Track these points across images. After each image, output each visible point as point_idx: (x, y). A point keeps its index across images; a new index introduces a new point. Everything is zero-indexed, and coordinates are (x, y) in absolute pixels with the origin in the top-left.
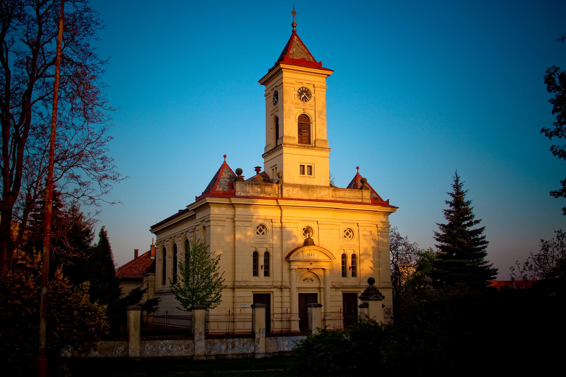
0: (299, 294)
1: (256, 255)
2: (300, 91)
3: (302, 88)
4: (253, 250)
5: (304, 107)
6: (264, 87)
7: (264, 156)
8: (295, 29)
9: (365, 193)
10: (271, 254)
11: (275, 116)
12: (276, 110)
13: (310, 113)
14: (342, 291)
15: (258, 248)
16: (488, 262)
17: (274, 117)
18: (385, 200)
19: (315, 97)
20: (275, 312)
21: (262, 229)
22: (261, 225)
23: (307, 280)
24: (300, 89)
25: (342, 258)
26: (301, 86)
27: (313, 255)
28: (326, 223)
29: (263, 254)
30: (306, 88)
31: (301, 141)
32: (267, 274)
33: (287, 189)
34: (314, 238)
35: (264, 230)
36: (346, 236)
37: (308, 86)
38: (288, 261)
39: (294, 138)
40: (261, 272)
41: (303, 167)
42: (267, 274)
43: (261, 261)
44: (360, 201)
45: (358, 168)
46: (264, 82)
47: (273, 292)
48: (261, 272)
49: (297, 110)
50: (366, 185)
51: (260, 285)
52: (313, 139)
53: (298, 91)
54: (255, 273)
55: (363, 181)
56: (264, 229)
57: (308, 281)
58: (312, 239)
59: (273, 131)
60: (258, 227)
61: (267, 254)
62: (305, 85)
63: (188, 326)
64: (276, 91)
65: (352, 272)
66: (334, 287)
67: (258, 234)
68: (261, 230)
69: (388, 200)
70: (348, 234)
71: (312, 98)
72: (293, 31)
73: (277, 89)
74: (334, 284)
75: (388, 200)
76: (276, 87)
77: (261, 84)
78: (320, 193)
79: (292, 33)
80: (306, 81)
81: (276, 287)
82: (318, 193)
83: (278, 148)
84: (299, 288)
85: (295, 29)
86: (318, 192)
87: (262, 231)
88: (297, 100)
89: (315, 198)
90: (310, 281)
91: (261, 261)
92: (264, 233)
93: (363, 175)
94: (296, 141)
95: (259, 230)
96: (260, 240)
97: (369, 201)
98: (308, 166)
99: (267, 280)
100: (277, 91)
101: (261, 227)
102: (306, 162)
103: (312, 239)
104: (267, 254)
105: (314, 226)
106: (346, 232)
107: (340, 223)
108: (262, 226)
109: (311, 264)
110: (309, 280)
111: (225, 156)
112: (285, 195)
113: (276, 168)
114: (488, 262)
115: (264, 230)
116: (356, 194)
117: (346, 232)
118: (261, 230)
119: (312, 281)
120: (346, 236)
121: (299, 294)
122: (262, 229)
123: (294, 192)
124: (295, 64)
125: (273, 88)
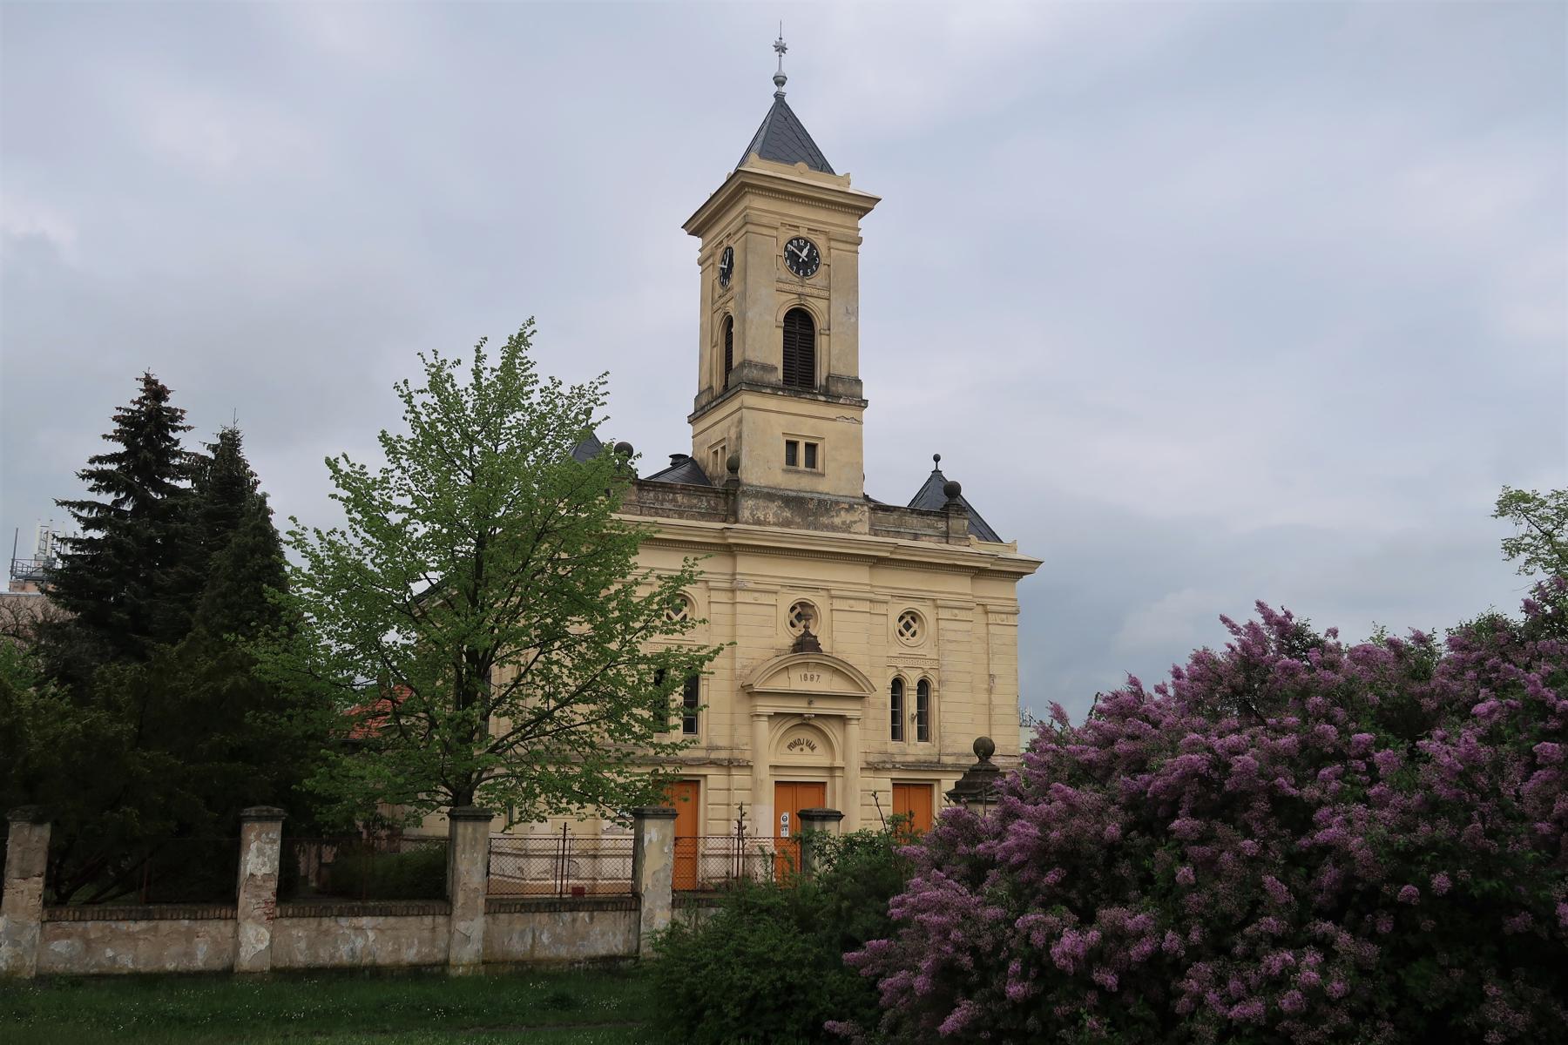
0: (776, 782)
1: (897, 684)
4: (892, 674)
5: (800, 290)
6: (697, 242)
7: (693, 420)
8: (784, 89)
9: (955, 521)
10: (934, 685)
11: (725, 314)
12: (728, 296)
13: (817, 307)
14: (892, 779)
15: (905, 670)
17: (722, 314)
20: (711, 830)
22: (908, 613)
23: (798, 748)
24: (791, 242)
25: (894, 691)
27: (816, 677)
32: (923, 735)
34: (819, 631)
35: (915, 626)
36: (904, 631)
37: (810, 236)
38: (749, 693)
40: (911, 729)
41: (792, 446)
42: (923, 735)
45: (937, 458)
46: (698, 226)
47: (705, 776)
48: (911, 729)
49: (784, 297)
50: (958, 501)
52: (820, 377)
54: (897, 733)
55: (953, 490)
56: (915, 622)
57: (802, 750)
58: (816, 637)
59: (719, 352)
61: (923, 685)
62: (803, 233)
63: (721, 848)
64: (727, 248)
65: (920, 729)
66: (873, 768)
70: (908, 626)
71: (822, 268)
72: (776, 95)
73: (731, 243)
74: (871, 759)
76: (728, 236)
77: (689, 234)
78: (837, 516)
79: (773, 100)
80: (807, 223)
81: (715, 763)
82: (833, 516)
83: (728, 395)
84: (776, 767)
85: (784, 89)
90: (807, 750)
92: (915, 632)
93: (950, 476)
95: (796, 617)
100: (730, 248)
101: (908, 618)
102: (805, 430)
103: (816, 637)
104: (923, 685)
105: (817, 600)
106: (904, 621)
107: (779, 588)
108: (911, 615)
110: (804, 746)
113: (724, 448)
115: (915, 626)
117: (904, 621)
118: (908, 626)
119: (813, 749)
120: (904, 631)
121: (776, 782)
125: (722, 241)
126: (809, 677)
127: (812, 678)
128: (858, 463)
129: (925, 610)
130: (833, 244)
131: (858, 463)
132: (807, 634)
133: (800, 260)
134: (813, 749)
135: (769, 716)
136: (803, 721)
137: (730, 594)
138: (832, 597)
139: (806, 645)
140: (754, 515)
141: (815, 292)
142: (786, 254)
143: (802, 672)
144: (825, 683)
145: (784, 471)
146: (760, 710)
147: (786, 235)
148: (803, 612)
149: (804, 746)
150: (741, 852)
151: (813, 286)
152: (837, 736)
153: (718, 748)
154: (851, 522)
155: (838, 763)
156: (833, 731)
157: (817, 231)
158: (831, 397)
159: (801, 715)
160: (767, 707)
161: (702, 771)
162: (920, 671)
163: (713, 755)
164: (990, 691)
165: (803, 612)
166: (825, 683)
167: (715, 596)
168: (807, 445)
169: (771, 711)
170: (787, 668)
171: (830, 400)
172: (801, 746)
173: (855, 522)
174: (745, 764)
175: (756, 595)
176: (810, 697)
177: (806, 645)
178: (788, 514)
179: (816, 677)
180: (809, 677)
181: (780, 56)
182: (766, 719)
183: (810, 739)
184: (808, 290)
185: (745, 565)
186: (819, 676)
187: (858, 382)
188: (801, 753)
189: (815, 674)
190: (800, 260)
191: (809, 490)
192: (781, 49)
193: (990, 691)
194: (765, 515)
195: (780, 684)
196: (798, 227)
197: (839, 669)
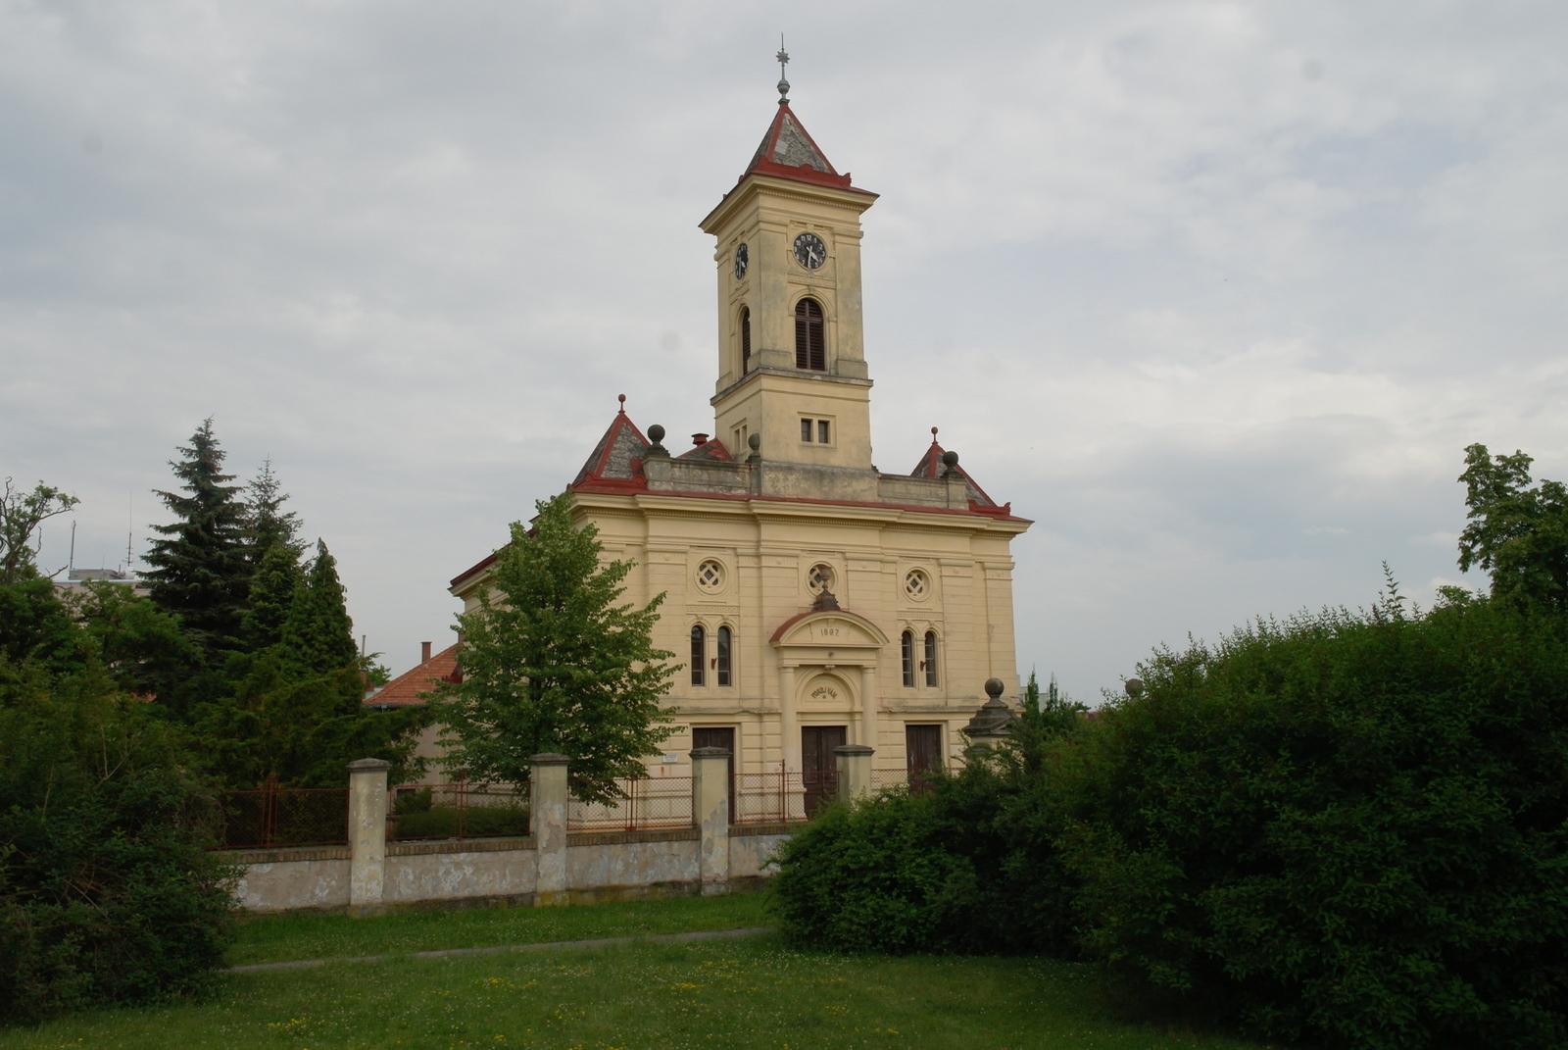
0: (803, 727)
1: (907, 636)
2: (799, 243)
3: (805, 235)
4: (692, 621)
5: (809, 281)
13: (825, 297)
18: (1000, 503)
21: (713, 570)
22: (709, 562)
24: (799, 238)
26: (802, 230)
27: (835, 632)
29: (716, 631)
30: (813, 237)
31: (801, 363)
33: (773, 475)
35: (717, 574)
39: (786, 354)
41: (807, 423)
44: (943, 505)
51: (709, 706)
53: (795, 243)
54: (908, 680)
60: (702, 567)
62: (810, 229)
67: (702, 582)
68: (709, 574)
69: (1008, 504)
75: (1008, 504)
84: (802, 713)
86: (846, 484)
87: (917, 584)
88: (793, 262)
89: (837, 497)
90: (829, 697)
91: (711, 651)
96: (706, 598)
97: (964, 507)
98: (820, 422)
101: (709, 567)
105: (835, 563)
106: (706, 570)
107: (973, 562)
109: (831, 655)
111: (622, 399)
115: (717, 574)
116: (933, 489)
117: (706, 570)
119: (834, 696)
120: (705, 579)
121: (803, 727)
122: (713, 570)
123: (790, 484)
127: (832, 633)
129: (929, 568)
130: (837, 238)
132: (826, 592)
134: (834, 696)
135: (795, 668)
136: (825, 672)
137: (756, 560)
138: (846, 559)
139: (825, 604)
141: (822, 283)
143: (823, 626)
144: (845, 636)
146: (786, 663)
147: (795, 232)
148: (821, 573)
149: (826, 694)
151: (822, 277)
152: (856, 683)
155: (858, 708)
156: (851, 678)
157: (822, 227)
158: (834, 379)
159: (822, 666)
160: (792, 659)
164: (989, 640)
165: (821, 573)
166: (845, 636)
167: (743, 561)
168: (820, 422)
169: (797, 663)
170: (809, 624)
173: (865, 490)
176: (831, 650)
177: (825, 604)
181: (783, 66)
182: (792, 670)
184: (816, 282)
185: (769, 532)
187: (864, 364)
192: (783, 58)
193: (989, 640)
196: (805, 224)
197: (857, 623)
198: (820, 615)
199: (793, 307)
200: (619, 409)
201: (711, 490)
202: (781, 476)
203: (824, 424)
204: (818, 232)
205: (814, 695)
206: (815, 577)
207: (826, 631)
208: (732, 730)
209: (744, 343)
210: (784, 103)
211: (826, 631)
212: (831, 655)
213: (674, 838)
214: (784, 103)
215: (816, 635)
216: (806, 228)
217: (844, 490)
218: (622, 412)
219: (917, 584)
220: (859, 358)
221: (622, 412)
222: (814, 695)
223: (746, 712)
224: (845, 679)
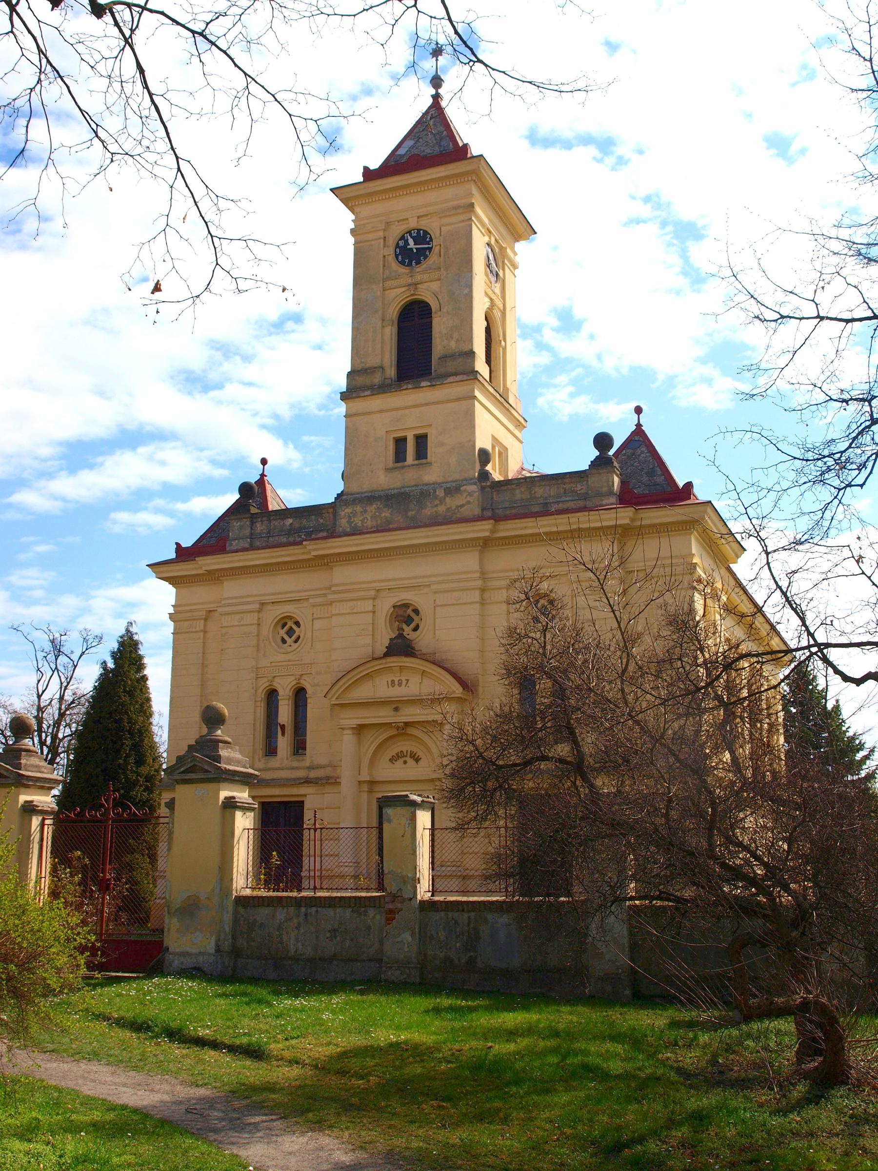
1: (272, 695)
4: (263, 684)
16: (427, 1011)
19: (418, 217)
23: (401, 760)
27: (404, 682)
28: (454, 585)
30: (419, 230)
32: (299, 747)
33: (349, 510)
36: (286, 637)
40: (284, 743)
41: (400, 442)
43: (285, 714)
48: (284, 743)
53: (398, 243)
54: (271, 750)
57: (405, 762)
61: (300, 694)
70: (290, 632)
82: (436, 506)
90: (410, 761)
91: (285, 714)
92: (299, 637)
94: (391, 372)
99: (295, 764)
104: (300, 694)
109: (396, 709)
112: (477, 592)
114: (427, 1011)
118: (290, 632)
120: (286, 637)
124: (611, 483)
126: (396, 683)
127: (400, 684)
128: (470, 441)
131: (470, 441)
133: (415, 251)
134: (418, 761)
140: (352, 522)
142: (398, 250)
145: (388, 470)
149: (408, 759)
150: (318, 873)
153: (319, 767)
154: (458, 507)
157: (427, 215)
161: (302, 790)
162: (293, 678)
163: (313, 774)
171: (434, 383)
172: (404, 759)
173: (462, 506)
174: (333, 781)
175: (350, 604)
176: (396, 705)
178: (386, 514)
179: (404, 682)
180: (396, 683)
182: (350, 732)
183: (414, 750)
186: (408, 680)
188: (404, 766)
189: (403, 679)
190: (415, 251)
191: (413, 484)
194: (362, 521)
195: (364, 692)
196: (407, 219)
198: (395, 661)
199: (393, 312)
200: (636, 422)
201: (291, 539)
202: (358, 508)
203: (421, 440)
204: (424, 224)
205: (392, 760)
206: (413, 620)
207: (393, 682)
208: (303, 802)
209: (490, 355)
210: (436, 97)
211: (393, 682)
212: (396, 709)
213: (266, 904)
214: (436, 97)
215: (381, 688)
216: (408, 223)
217: (435, 509)
218: (639, 425)
219: (413, 620)
220: (466, 348)
221: (639, 425)
222: (392, 760)
223: (307, 781)
224: (425, 738)
